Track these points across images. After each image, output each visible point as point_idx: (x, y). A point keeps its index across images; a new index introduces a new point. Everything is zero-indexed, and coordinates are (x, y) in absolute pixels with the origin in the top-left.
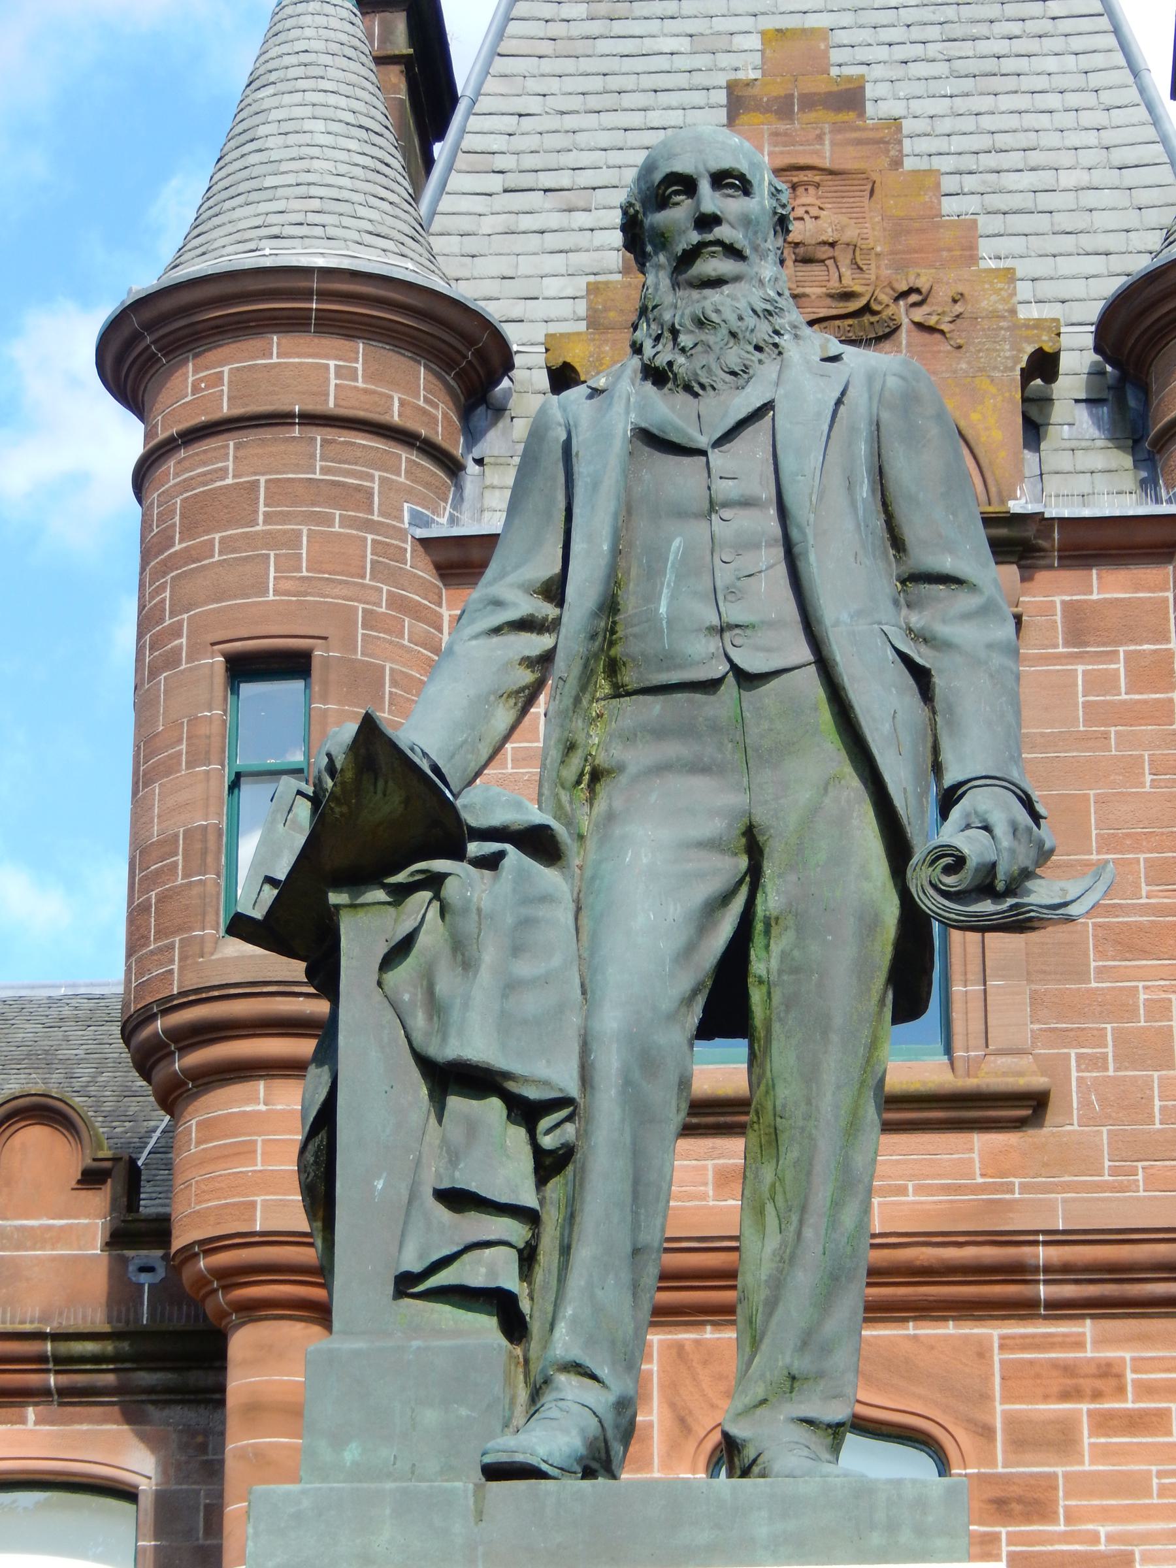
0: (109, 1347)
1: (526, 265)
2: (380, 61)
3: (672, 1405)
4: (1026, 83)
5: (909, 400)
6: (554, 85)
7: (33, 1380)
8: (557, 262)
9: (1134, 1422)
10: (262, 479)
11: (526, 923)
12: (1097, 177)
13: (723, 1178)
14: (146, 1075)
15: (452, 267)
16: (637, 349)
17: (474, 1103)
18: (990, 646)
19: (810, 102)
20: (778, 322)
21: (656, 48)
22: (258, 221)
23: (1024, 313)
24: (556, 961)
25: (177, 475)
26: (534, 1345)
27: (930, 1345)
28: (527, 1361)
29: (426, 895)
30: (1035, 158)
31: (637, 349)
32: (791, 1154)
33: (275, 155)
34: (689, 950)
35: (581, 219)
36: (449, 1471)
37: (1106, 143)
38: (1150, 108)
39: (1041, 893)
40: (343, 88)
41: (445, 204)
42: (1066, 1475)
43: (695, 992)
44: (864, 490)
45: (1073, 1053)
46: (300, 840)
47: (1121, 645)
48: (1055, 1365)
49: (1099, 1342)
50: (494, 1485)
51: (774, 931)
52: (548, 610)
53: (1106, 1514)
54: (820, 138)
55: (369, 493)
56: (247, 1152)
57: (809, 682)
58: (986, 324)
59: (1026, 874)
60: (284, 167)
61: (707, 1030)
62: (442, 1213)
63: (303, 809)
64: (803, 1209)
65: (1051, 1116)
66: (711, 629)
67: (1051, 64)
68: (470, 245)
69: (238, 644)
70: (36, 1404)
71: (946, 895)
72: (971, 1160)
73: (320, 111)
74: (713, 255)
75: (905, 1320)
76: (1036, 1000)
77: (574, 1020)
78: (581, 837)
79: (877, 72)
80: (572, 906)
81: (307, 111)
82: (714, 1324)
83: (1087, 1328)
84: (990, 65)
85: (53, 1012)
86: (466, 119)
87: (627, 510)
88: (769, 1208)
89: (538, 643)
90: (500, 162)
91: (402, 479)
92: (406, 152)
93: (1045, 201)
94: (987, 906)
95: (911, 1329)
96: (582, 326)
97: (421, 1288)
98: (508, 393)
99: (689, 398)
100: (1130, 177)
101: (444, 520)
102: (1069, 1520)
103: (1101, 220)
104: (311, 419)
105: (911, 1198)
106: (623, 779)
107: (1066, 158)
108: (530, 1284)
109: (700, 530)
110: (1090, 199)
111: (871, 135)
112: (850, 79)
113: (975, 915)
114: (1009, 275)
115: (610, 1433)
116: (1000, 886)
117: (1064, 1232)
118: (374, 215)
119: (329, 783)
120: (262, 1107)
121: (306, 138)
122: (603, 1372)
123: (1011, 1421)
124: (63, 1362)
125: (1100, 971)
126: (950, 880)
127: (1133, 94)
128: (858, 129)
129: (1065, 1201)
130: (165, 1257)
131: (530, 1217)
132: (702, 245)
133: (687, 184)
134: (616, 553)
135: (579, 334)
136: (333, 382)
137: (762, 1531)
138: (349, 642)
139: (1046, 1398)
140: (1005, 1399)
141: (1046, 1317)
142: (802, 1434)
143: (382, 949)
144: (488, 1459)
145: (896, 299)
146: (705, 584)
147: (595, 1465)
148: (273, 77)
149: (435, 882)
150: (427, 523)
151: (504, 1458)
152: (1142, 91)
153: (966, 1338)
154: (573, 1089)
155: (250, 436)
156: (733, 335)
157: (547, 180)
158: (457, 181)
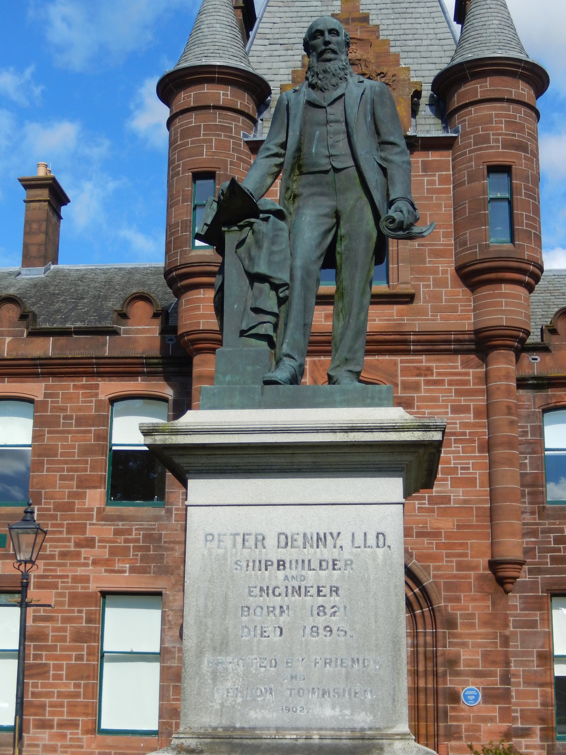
0: (161, 361)
1: (275, 65)
2: (235, 8)
3: (312, 377)
4: (414, 15)
5: (382, 94)
6: (283, 15)
7: (140, 369)
8: (284, 65)
9: (436, 383)
10: (202, 124)
11: (276, 236)
12: (433, 42)
13: (327, 317)
14: (171, 288)
15: (254, 66)
16: (307, 79)
17: (261, 284)
18: (403, 162)
19: (354, 20)
20: (347, 71)
21: (312, 5)
22: (201, 52)
23: (412, 80)
24: (284, 246)
25: (179, 123)
26: (277, 350)
27: (381, 362)
28: (275, 354)
29: (249, 228)
30: (416, 37)
31: (307, 79)
32: (347, 299)
33: (206, 34)
34: (319, 244)
35: (290, 52)
36: (253, 383)
37: (436, 32)
38: (448, 23)
39: (416, 229)
40: (225, 15)
41: (253, 48)
42: (417, 396)
43: (321, 255)
44: (369, 119)
45: (421, 284)
46: (214, 213)
47: (437, 172)
48: (415, 367)
49: (427, 361)
50: (266, 386)
51: (343, 239)
52: (282, 151)
53: (427, 407)
54: (357, 30)
55: (232, 128)
56: (198, 308)
57: (353, 171)
58: (402, 83)
59: (412, 225)
60: (208, 37)
61: (324, 267)
62: (252, 314)
63: (215, 205)
64: (350, 315)
65: (415, 301)
66: (327, 156)
67: (421, 10)
68: (260, 59)
69: (195, 170)
70: (141, 376)
71: (390, 229)
72: (393, 312)
73: (219, 21)
74: (328, 53)
75: (375, 355)
76: (412, 269)
77: (289, 262)
78: (290, 213)
79: (373, 12)
80: (288, 232)
81: (215, 21)
82: (323, 355)
83: (424, 358)
84: (404, 10)
85: (145, 272)
86: (259, 24)
87: (304, 123)
88: (341, 315)
89: (279, 160)
90: (268, 36)
91: (241, 124)
92: (242, 33)
93: (419, 49)
94: (401, 233)
95: (376, 357)
96: (290, 82)
97: (247, 334)
98: (270, 100)
99: (321, 92)
100: (442, 42)
101: (252, 136)
102: (418, 408)
103: (434, 54)
104: (216, 108)
105: (377, 322)
106: (302, 198)
107: (424, 37)
108: (276, 333)
109: (324, 129)
110: (431, 48)
111: (371, 29)
112: (365, 13)
113: (398, 235)
114: (408, 69)
115: (297, 374)
116: (405, 227)
117: (418, 332)
118: (233, 51)
119: (222, 198)
120: (202, 296)
121: (214, 29)
122: (296, 357)
123: (403, 382)
124: (148, 365)
125: (430, 262)
126: (391, 225)
127: (444, 19)
128: (367, 28)
129: (418, 323)
130: (176, 337)
131: (276, 315)
132: (325, 50)
133: (321, 33)
134: (301, 135)
135: (289, 84)
136: (222, 97)
137: (338, 399)
138: (226, 169)
139: (412, 376)
140: (402, 376)
141: (413, 355)
142: (348, 374)
143: (236, 243)
144: (265, 379)
145: (377, 76)
146: (325, 143)
147: (293, 382)
148: (205, 12)
149: (251, 225)
150: (247, 137)
151: (269, 379)
152: (446, 18)
153: (391, 360)
154: (288, 281)
155: (198, 112)
156: (334, 75)
157: (281, 41)
158: (256, 42)
